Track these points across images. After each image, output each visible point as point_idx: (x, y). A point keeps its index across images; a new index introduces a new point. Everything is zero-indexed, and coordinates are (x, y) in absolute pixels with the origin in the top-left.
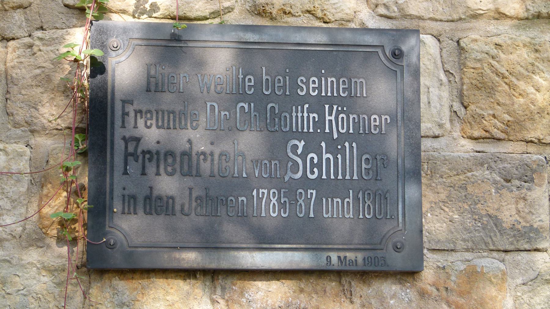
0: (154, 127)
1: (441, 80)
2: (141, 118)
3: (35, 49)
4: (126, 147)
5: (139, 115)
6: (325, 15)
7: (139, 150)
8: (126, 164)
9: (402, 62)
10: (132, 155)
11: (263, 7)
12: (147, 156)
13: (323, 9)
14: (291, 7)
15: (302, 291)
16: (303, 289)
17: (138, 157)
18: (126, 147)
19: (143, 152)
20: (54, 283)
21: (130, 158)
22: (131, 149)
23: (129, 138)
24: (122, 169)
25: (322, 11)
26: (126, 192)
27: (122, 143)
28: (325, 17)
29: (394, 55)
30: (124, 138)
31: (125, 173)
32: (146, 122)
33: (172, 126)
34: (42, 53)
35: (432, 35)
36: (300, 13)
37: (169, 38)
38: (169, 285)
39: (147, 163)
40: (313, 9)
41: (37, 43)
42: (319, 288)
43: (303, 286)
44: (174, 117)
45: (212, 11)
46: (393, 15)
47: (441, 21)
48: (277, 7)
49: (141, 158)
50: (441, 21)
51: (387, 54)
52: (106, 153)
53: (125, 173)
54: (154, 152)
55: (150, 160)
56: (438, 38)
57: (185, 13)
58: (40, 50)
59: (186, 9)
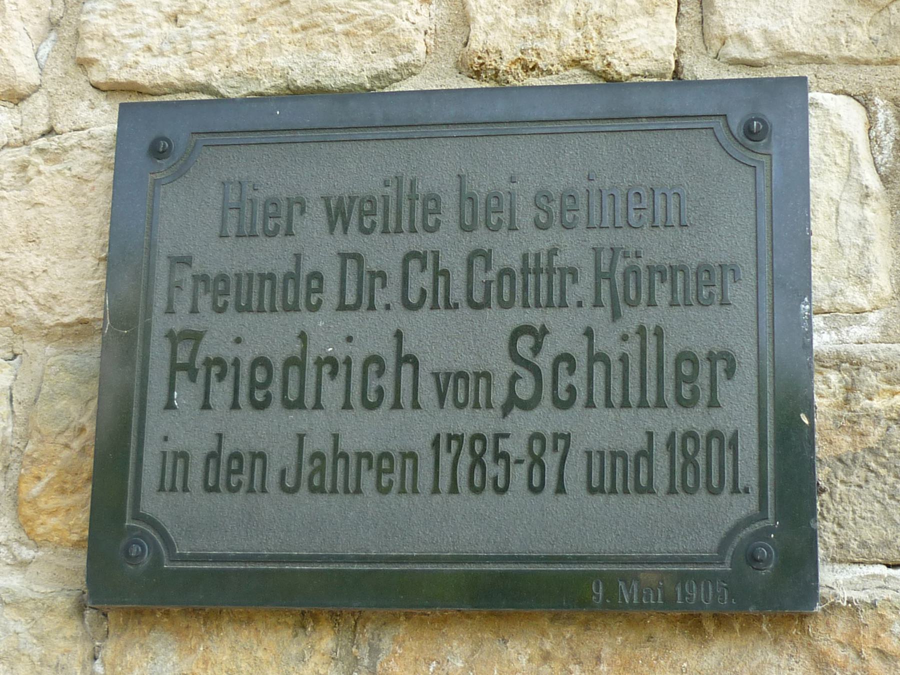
0: (231, 308)
1: (867, 187)
2: (206, 291)
3: (31, 171)
4: (174, 353)
5: (201, 286)
6: (609, 65)
7: (200, 359)
8: (172, 388)
9: (768, 145)
10: (183, 367)
11: (479, 58)
12: (215, 370)
13: (604, 53)
14: (538, 54)
15: (546, 657)
16: (548, 653)
17: (196, 371)
18: (174, 353)
19: (208, 363)
20: (32, 635)
21: (181, 375)
22: (183, 357)
23: (181, 333)
24: (164, 399)
25: (604, 57)
26: (170, 447)
27: (166, 345)
28: (609, 70)
29: (749, 132)
30: (170, 335)
31: (170, 406)
32: (215, 303)
33: (266, 306)
34: (42, 177)
35: (849, 95)
36: (557, 67)
37: (467, 190)
38: (260, 642)
39: (214, 386)
40: (583, 55)
41: (37, 159)
42: (585, 651)
43: (548, 646)
44: (273, 287)
45: (374, 73)
46: (759, 56)
47: (867, 63)
48: (509, 56)
49: (201, 373)
50: (867, 63)
51: (735, 132)
52: (776, 419)
53: (170, 406)
54: (229, 361)
55: (221, 377)
56: (865, 101)
57: (317, 81)
58: (39, 172)
59: (321, 73)
